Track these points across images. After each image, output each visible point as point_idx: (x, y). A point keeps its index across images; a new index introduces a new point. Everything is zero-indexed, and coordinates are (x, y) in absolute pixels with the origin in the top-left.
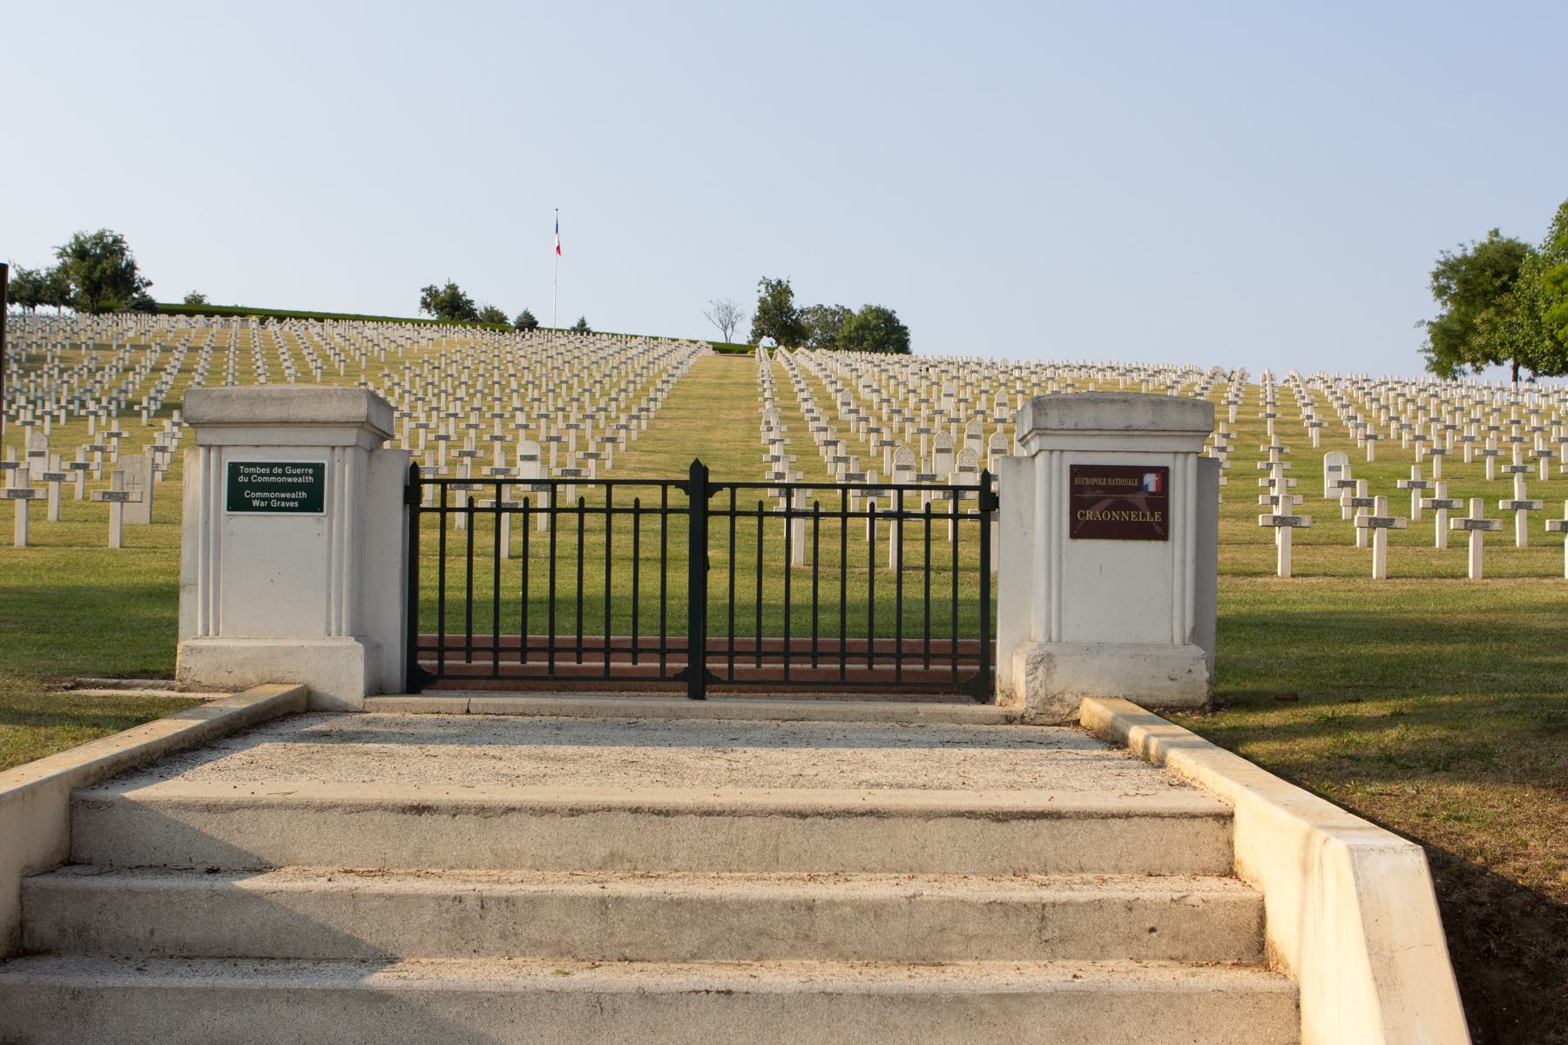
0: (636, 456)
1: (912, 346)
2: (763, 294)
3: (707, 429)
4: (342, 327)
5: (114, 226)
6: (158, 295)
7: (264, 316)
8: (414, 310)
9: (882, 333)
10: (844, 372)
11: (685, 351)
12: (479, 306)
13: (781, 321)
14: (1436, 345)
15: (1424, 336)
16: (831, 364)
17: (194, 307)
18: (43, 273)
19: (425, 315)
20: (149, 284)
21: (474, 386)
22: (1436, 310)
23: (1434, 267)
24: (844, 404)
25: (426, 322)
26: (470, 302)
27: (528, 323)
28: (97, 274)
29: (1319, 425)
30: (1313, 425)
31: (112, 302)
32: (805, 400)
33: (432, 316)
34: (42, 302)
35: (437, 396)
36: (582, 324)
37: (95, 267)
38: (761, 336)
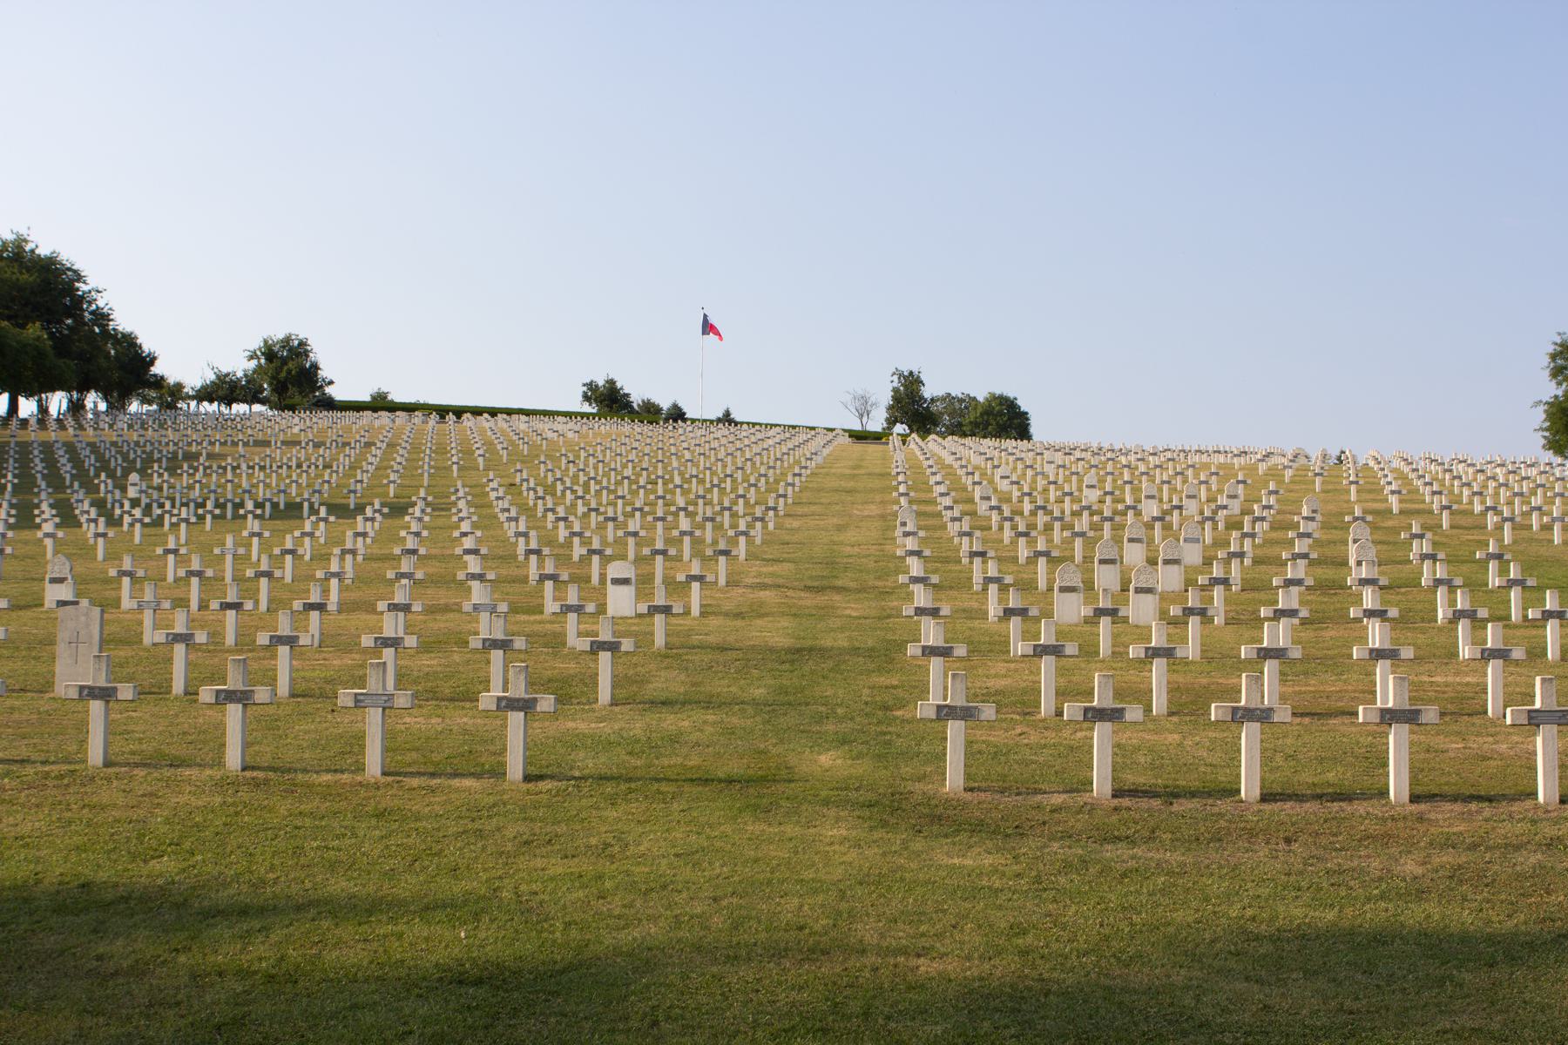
0: (757, 567)
1: (1033, 430)
2: (896, 384)
3: (840, 528)
5: (300, 331)
6: (337, 392)
7: (442, 411)
9: (1004, 420)
10: (977, 460)
11: (820, 440)
12: (636, 399)
13: (914, 409)
14: (1553, 423)
15: (1539, 416)
16: (961, 451)
17: (380, 404)
18: (240, 374)
19: (587, 408)
20: (331, 383)
22: (171, 381)
23: (1551, 349)
24: (982, 498)
26: (628, 395)
27: (677, 415)
28: (283, 374)
29: (1399, 492)
30: (1393, 492)
31: (297, 399)
32: (938, 483)
34: (237, 401)
36: (727, 414)
37: (281, 368)
38: (894, 423)
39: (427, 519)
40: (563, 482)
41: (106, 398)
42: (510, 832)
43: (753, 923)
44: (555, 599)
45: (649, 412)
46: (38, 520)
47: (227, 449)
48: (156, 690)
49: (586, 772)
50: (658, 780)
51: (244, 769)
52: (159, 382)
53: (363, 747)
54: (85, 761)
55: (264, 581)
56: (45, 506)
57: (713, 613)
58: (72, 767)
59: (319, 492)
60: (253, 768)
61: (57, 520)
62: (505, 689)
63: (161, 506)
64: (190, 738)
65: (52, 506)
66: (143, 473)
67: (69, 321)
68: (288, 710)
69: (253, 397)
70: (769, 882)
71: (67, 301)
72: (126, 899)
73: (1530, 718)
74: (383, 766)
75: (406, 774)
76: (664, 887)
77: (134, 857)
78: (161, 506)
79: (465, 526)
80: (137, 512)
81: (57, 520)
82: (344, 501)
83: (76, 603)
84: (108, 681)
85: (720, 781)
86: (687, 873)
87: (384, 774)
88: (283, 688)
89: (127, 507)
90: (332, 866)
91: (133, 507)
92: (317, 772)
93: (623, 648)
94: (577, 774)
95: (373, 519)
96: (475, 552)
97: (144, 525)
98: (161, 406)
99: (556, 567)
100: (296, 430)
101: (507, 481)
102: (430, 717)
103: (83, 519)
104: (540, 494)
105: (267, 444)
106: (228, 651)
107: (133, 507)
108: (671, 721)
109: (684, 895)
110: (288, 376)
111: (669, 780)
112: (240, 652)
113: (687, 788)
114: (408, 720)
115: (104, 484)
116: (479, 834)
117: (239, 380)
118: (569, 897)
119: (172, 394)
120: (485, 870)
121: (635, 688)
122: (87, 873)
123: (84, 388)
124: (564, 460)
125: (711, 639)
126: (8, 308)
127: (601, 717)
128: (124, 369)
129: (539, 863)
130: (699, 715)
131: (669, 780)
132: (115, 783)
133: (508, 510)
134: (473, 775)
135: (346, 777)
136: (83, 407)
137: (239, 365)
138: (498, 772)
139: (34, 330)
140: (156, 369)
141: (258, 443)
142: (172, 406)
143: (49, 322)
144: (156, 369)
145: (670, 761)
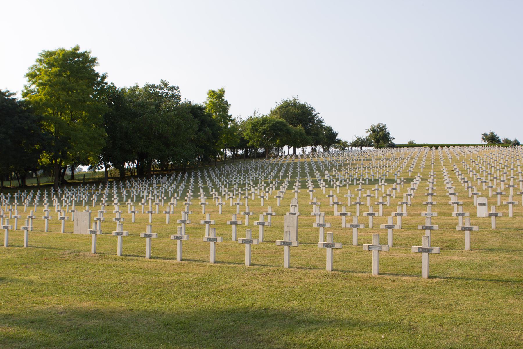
4: (468, 148)
6: (396, 142)
7: (431, 146)
8: (480, 141)
12: (502, 139)
17: (411, 145)
18: (364, 137)
19: (484, 143)
20: (394, 139)
21: (510, 167)
22: (343, 141)
25: (484, 145)
26: (498, 137)
28: (378, 137)
31: (383, 144)
33: (486, 143)
34: (363, 146)
35: (495, 172)
39: (435, 183)
40: (482, 169)
41: (323, 148)
42: (415, 298)
43: (497, 341)
45: (507, 143)
46: (307, 186)
47: (357, 162)
48: (346, 243)
49: (452, 276)
50: (478, 280)
51: (332, 271)
52: (339, 142)
53: (371, 263)
54: (283, 266)
55: (358, 206)
56: (309, 182)
57: (518, 216)
58: (278, 268)
59: (397, 175)
60: (335, 270)
61: (313, 186)
63: (345, 181)
64: (319, 259)
65: (312, 182)
66: (330, 171)
67: (311, 124)
68: (355, 250)
69: (369, 145)
70: (510, 324)
71: (309, 117)
72: (276, 315)
73: (369, 248)
74: (378, 271)
75: (386, 274)
76: (467, 323)
77: (285, 299)
78: (345, 181)
79: (449, 185)
80: (338, 183)
81: (313, 186)
82: (393, 178)
85: (503, 281)
86: (478, 318)
87: (379, 274)
88: (261, 239)
90: (348, 307)
91: (336, 181)
92: (356, 272)
93: (474, 230)
94: (448, 276)
95: (416, 184)
96: (454, 194)
97: (326, 188)
99: (458, 200)
100: (381, 155)
101: (450, 169)
102: (402, 253)
103: (321, 186)
104: (475, 173)
105: (371, 160)
106: (342, 229)
107: (336, 181)
108: (491, 257)
109: (474, 327)
110: (380, 138)
111: (482, 280)
112: (249, 227)
113: (490, 283)
114: (394, 254)
115: (318, 174)
116: (405, 298)
117: (364, 139)
118: (429, 325)
119: (343, 145)
120: (401, 312)
121: (480, 244)
122: (268, 305)
123: (316, 145)
124: (471, 161)
125: (515, 226)
126: (292, 121)
127: (465, 256)
128: (329, 139)
129: (423, 310)
130: (502, 255)
131: (482, 280)
132: (290, 274)
133: (464, 179)
134: (410, 275)
135: (365, 275)
137: (364, 135)
138: (419, 275)
139: (300, 127)
140: (338, 137)
141: (368, 160)
142: (343, 149)
143: (304, 124)
144: (338, 137)
145: (486, 273)
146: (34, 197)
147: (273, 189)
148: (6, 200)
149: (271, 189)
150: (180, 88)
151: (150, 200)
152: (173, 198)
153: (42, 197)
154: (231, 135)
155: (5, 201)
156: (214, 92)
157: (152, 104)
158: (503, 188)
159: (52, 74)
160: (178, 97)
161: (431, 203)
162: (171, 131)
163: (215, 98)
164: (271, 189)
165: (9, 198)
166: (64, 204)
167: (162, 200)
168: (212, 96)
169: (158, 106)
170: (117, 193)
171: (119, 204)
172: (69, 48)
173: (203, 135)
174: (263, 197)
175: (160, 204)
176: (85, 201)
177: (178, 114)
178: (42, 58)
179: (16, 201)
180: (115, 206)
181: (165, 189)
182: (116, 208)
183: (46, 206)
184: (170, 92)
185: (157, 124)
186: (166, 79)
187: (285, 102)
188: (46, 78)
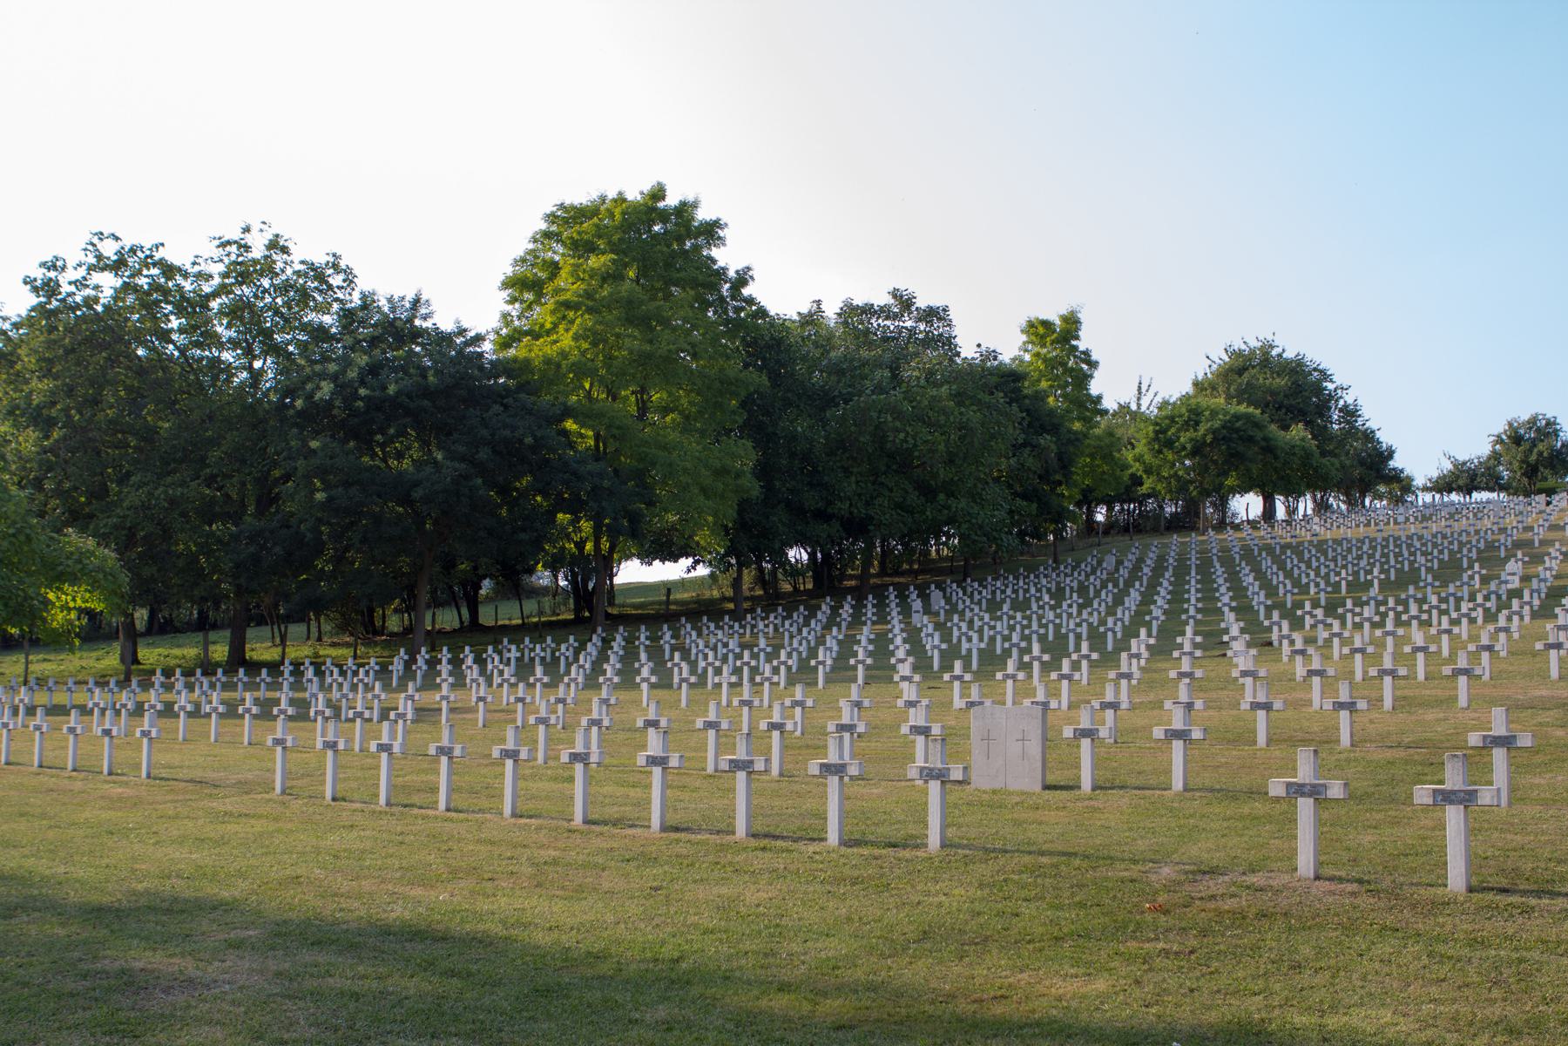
27: (1278, 426)
28: (1533, 457)
34: (1478, 489)
37: (1531, 450)
44: (961, 697)
62: (926, 761)
69: (1494, 484)
83: (981, 703)
84: (748, 754)
89: (1308, 607)
98: (1390, 500)
128: (1364, 468)
136: (1450, 492)
137: (1476, 447)
146: (603, 657)
147: (1522, 618)
148: (506, 669)
149: (1516, 618)
150: (953, 315)
151: (1036, 664)
152: (1124, 655)
153: (630, 656)
154: (1103, 458)
155: (501, 673)
156: (1046, 324)
157: (878, 364)
158: (1367, 638)
159: (593, 273)
160: (948, 342)
161: (1190, 675)
162: (942, 447)
163: (1053, 342)
164: (1516, 618)
165: (513, 662)
166: (497, 680)
167: (1084, 663)
168: (1043, 337)
169: (894, 369)
170: (905, 641)
171: (917, 678)
172: (634, 193)
173: (1031, 460)
174: (1490, 648)
175: (1077, 676)
176: (789, 668)
177: (958, 394)
178: (554, 228)
179: (539, 670)
180: (905, 685)
181: (1090, 625)
182: (909, 691)
183: (445, 686)
184: (922, 326)
185: (898, 424)
186: (905, 285)
187: (1236, 355)
188: (580, 287)
